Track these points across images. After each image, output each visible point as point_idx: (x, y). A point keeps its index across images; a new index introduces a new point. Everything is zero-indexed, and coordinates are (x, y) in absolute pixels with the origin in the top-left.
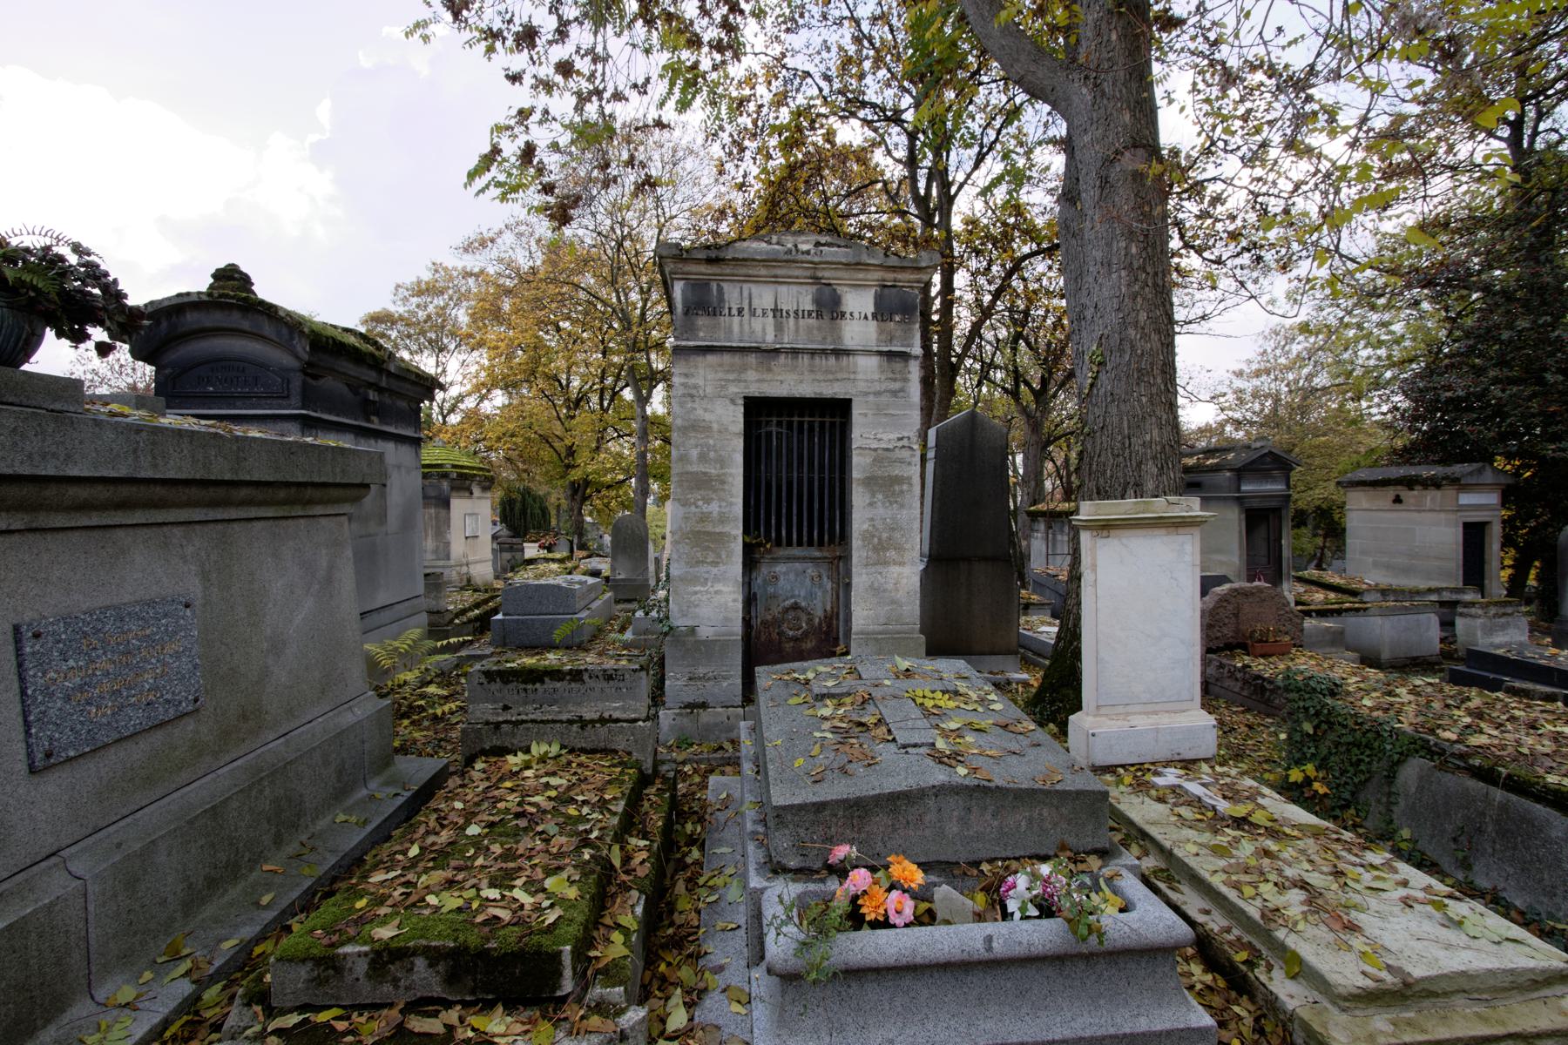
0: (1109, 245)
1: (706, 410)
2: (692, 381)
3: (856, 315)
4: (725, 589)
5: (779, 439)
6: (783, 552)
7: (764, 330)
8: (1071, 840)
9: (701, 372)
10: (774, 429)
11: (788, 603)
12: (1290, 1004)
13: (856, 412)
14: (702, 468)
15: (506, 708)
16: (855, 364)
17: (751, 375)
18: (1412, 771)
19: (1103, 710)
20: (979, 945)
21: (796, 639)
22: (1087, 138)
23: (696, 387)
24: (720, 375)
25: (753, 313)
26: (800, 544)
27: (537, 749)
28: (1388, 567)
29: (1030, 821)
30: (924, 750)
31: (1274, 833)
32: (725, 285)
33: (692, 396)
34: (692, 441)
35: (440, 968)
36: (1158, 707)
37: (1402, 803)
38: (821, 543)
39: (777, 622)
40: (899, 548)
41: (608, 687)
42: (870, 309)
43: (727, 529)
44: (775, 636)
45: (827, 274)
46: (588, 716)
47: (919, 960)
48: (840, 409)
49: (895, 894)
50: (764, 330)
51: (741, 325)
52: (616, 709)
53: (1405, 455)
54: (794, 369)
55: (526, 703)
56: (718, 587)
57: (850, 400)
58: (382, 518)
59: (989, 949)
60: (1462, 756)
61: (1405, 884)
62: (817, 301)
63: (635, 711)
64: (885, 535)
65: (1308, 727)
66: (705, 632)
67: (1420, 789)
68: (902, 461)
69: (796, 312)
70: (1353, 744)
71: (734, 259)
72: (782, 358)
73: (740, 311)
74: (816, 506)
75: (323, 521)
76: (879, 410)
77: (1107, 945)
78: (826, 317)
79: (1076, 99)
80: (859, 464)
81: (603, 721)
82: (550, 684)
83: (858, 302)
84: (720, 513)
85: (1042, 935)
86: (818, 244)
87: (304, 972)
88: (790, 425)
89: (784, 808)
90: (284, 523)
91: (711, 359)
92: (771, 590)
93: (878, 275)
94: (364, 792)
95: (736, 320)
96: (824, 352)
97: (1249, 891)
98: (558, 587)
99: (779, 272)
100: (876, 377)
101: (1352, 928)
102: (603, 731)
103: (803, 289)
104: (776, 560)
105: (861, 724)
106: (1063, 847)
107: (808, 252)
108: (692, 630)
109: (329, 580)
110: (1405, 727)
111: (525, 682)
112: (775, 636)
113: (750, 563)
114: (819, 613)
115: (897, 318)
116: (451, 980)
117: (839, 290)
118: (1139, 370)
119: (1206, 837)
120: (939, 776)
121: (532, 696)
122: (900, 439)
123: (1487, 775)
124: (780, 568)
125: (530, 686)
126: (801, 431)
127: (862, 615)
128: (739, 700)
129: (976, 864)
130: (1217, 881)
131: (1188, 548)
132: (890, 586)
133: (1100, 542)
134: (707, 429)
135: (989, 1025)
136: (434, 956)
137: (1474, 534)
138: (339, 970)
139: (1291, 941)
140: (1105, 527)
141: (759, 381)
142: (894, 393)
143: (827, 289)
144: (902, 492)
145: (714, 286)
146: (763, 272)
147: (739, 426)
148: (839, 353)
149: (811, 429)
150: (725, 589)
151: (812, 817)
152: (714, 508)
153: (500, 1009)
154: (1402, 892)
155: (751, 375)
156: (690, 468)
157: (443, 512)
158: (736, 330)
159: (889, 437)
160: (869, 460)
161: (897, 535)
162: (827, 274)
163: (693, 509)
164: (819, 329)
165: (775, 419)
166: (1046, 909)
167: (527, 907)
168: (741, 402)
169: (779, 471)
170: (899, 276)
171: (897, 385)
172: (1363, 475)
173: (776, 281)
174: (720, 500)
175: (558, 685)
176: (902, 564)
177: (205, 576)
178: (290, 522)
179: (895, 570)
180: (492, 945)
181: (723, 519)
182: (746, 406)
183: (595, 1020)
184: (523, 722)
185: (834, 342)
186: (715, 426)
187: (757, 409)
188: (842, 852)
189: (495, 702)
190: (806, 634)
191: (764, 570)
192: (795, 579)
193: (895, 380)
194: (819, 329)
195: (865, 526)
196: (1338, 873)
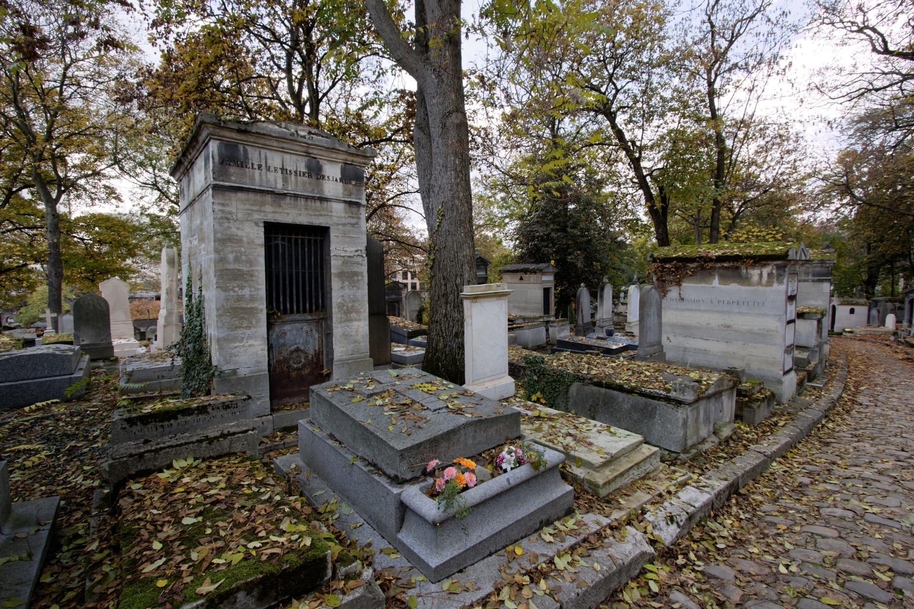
0: (446, 157)
1: (238, 229)
2: (227, 209)
3: (331, 178)
5: (284, 249)
6: (288, 317)
8: (510, 436)
9: (234, 203)
10: (280, 242)
11: (293, 348)
12: (582, 476)
13: (333, 234)
14: (237, 266)
15: (146, 442)
16: (331, 207)
18: (574, 388)
20: (506, 483)
21: (298, 369)
22: (434, 101)
23: (230, 213)
25: (268, 169)
26: (298, 312)
27: (179, 464)
28: (518, 308)
30: (444, 410)
31: (551, 419)
32: (249, 149)
33: (228, 219)
34: (229, 249)
35: (255, 593)
37: (571, 400)
39: (286, 360)
40: (358, 312)
41: (227, 413)
43: (255, 305)
44: (285, 369)
45: (315, 152)
46: (212, 435)
47: (488, 497)
48: (323, 232)
49: (467, 474)
50: (276, 181)
52: (233, 426)
53: (521, 259)
54: (295, 207)
56: (251, 342)
57: (329, 228)
59: (509, 483)
60: (590, 379)
61: (595, 426)
62: (308, 167)
63: (246, 425)
64: (350, 305)
65: (535, 378)
66: (243, 372)
67: (577, 394)
69: (296, 172)
70: (555, 381)
71: (257, 133)
72: (288, 200)
73: (260, 167)
74: (307, 289)
77: (548, 466)
78: (314, 177)
79: (429, 80)
80: (335, 265)
81: (223, 436)
82: (181, 419)
83: (332, 171)
85: (524, 472)
86: (310, 133)
88: (290, 240)
89: (404, 450)
91: (240, 195)
92: (282, 341)
93: (344, 157)
95: (257, 172)
96: (313, 198)
97: (556, 441)
99: (285, 146)
100: (343, 215)
101: (591, 444)
102: (225, 443)
103: (300, 158)
104: (284, 323)
105: (404, 405)
106: (507, 439)
107: (304, 137)
108: (234, 372)
110: (570, 371)
112: (285, 369)
113: (270, 326)
114: (311, 352)
117: (321, 162)
119: (530, 426)
120: (461, 420)
121: (168, 430)
123: (599, 384)
124: (287, 327)
125: (166, 423)
127: (340, 350)
128: (268, 411)
129: (480, 455)
130: (543, 441)
132: (354, 333)
133: (474, 305)
134: (240, 241)
135: (510, 516)
136: (248, 588)
137: (546, 291)
139: (576, 454)
140: (475, 298)
141: (273, 212)
142: (353, 225)
143: (314, 161)
145: (241, 148)
146: (275, 144)
147: (261, 239)
148: (322, 199)
149: (303, 243)
152: (246, 292)
153: (295, 601)
154: (595, 429)
155: (268, 208)
156: (228, 266)
158: (258, 179)
159: (350, 250)
160: (340, 262)
161: (356, 304)
162: (315, 152)
163: (232, 293)
164: (310, 184)
165: (280, 236)
166: (519, 462)
167: (286, 543)
168: (262, 225)
169: (284, 268)
170: (355, 159)
171: (354, 221)
172: (508, 267)
173: (283, 151)
174: (250, 287)
175: (189, 418)
176: (359, 320)
179: (356, 324)
180: (285, 566)
182: (265, 227)
183: (351, 583)
184: (161, 449)
186: (245, 239)
187: (272, 229)
188: (434, 463)
190: (304, 366)
191: (277, 329)
192: (298, 334)
193: (353, 218)
196: (576, 428)
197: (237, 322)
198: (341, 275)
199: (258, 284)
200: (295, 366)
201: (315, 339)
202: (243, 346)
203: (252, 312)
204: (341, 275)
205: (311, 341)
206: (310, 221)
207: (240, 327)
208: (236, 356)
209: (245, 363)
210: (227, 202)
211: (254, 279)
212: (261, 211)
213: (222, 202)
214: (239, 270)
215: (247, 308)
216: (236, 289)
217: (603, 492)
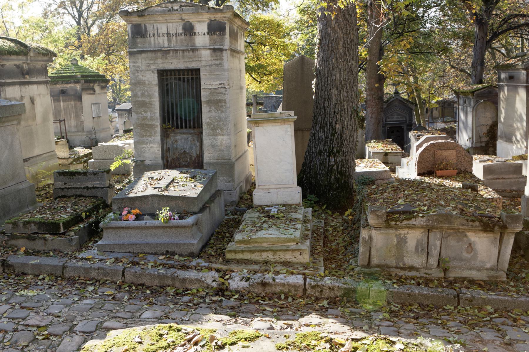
1: (143, 76)
2: (137, 65)
3: (200, 33)
4: (155, 146)
7: (163, 42)
9: (140, 60)
10: (173, 81)
15: (65, 184)
16: (201, 54)
17: (160, 61)
19: (260, 187)
23: (138, 67)
24: (148, 62)
26: (186, 127)
29: (176, 204)
33: (137, 71)
34: (138, 89)
36: (281, 186)
38: (194, 128)
42: (206, 30)
43: (154, 123)
46: (89, 186)
50: (163, 42)
51: (154, 40)
55: (70, 182)
56: (152, 145)
58: (34, 118)
64: (216, 124)
68: (221, 93)
73: (154, 35)
76: (211, 73)
80: (204, 95)
81: (94, 188)
84: (151, 116)
87: (11, 225)
92: (175, 146)
94: (28, 209)
95: (152, 38)
96: (187, 50)
98: (118, 146)
100: (210, 59)
102: (94, 190)
103: (178, 24)
113: (165, 134)
114: (195, 155)
115: (217, 34)
116: (39, 228)
117: (193, 23)
118: (332, 47)
122: (221, 84)
124: (178, 137)
131: (289, 130)
132: (219, 144)
134: (144, 83)
138: (17, 226)
142: (217, 65)
152: (148, 114)
155: (160, 61)
157: (78, 104)
158: (153, 42)
160: (208, 93)
161: (221, 123)
163: (140, 115)
164: (185, 40)
168: (156, 72)
171: (217, 62)
175: (80, 177)
176: (223, 135)
179: (220, 138)
182: (158, 73)
184: (70, 188)
185: (192, 46)
186: (147, 82)
187: (163, 74)
189: (61, 182)
193: (217, 60)
194: (185, 40)
195: (208, 120)
200: (183, 163)
202: (148, 147)
204: (209, 102)
205: (194, 147)
206: (186, 66)
207: (145, 136)
208: (144, 153)
209: (149, 158)
211: (153, 106)
214: (144, 101)
216: (143, 113)
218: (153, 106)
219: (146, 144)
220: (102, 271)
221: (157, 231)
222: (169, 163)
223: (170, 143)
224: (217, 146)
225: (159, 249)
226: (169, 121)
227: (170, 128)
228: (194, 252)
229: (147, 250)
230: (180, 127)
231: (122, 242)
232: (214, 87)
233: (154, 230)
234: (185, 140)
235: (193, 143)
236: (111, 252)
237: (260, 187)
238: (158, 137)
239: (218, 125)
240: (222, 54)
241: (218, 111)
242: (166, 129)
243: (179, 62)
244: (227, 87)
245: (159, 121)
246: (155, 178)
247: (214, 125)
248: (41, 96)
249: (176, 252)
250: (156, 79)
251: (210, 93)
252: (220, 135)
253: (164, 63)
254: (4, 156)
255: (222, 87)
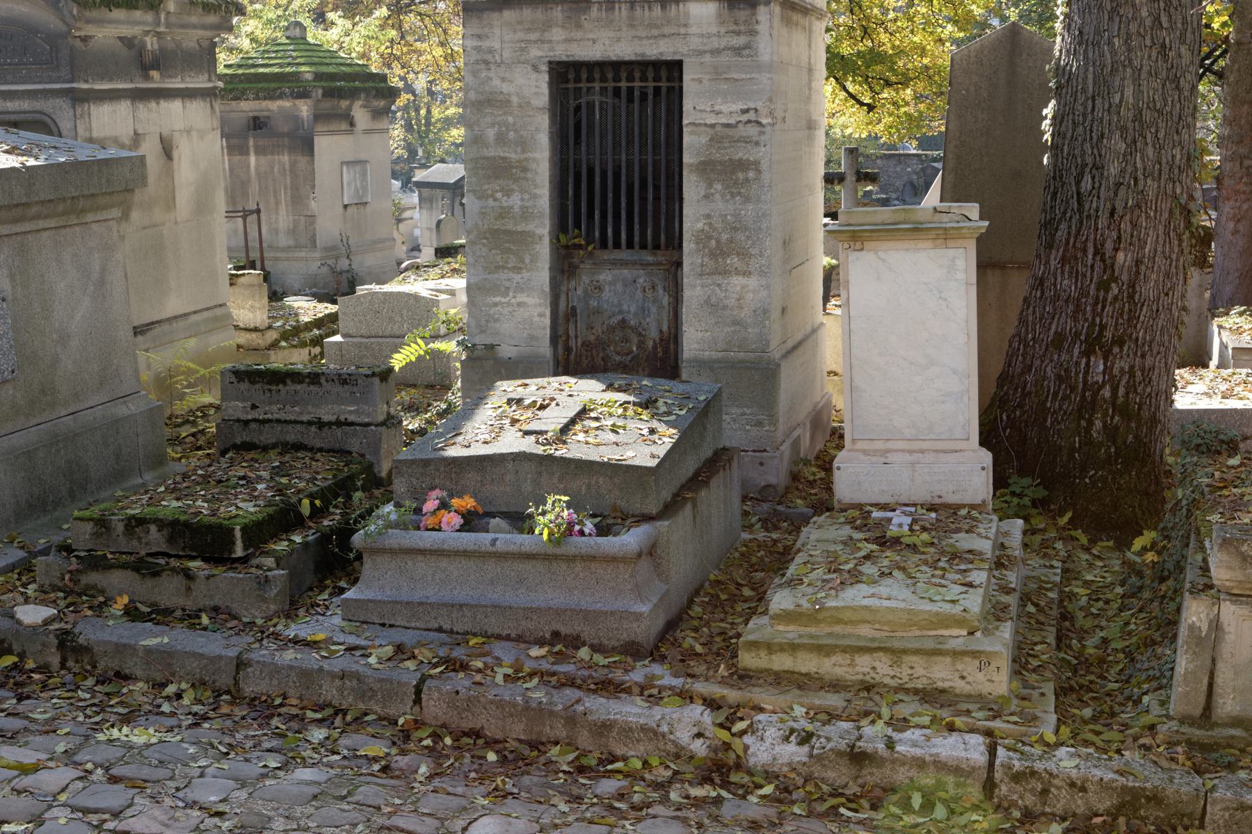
1: (503, 80)
2: (486, 44)
4: (530, 301)
6: (606, 255)
9: (497, 31)
10: (597, 99)
11: (615, 320)
15: (254, 407)
16: (687, 14)
17: (557, 34)
19: (859, 445)
23: (491, 51)
24: (520, 35)
26: (630, 245)
29: (589, 486)
33: (487, 63)
34: (488, 120)
36: (925, 445)
38: (657, 247)
41: (344, 391)
43: (530, 227)
46: (326, 418)
48: (668, 73)
52: (351, 412)
56: (522, 298)
58: (170, 202)
63: (368, 415)
64: (725, 237)
68: (747, 141)
75: (95, 227)
76: (717, 74)
80: (693, 144)
81: (339, 423)
82: (292, 387)
84: (522, 207)
90: (63, 231)
94: (140, 481)
98: (416, 297)
100: (714, 30)
109: (102, 282)
111: (269, 383)
114: (654, 334)
116: (171, 540)
124: (605, 276)
126: (630, 100)
131: (961, 263)
132: (732, 302)
142: (738, 51)
144: (747, 180)
149: (644, 97)
150: (530, 301)
151: (420, 470)
152: (515, 201)
155: (557, 34)
157: (302, 161)
160: (704, 140)
161: (741, 236)
163: (491, 202)
168: (545, 68)
171: (740, 41)
174: (523, 191)
175: (299, 387)
176: (747, 274)
177: (12, 277)
178: (68, 230)
179: (737, 281)
181: (526, 215)
184: (269, 421)
186: (515, 100)
187: (565, 75)
189: (244, 401)
192: (617, 285)
193: (738, 33)
195: (700, 225)
197: (498, 258)
198: (706, 168)
199: (536, 186)
200: (618, 358)
201: (661, 307)
202: (508, 304)
203: (525, 239)
204: (706, 168)
205: (654, 310)
206: (639, 50)
207: (503, 267)
208: (497, 320)
210: (486, 30)
211: (529, 175)
212: (543, 42)
213: (478, 31)
214: (504, 159)
215: (517, 232)
216: (499, 195)
217: (747, 659)
218: (529, 175)
219: (506, 294)
220: (355, 682)
221: (528, 566)
222: (572, 357)
223: (579, 292)
224: (725, 307)
225: (531, 625)
226: (577, 225)
227: (579, 247)
228: (639, 639)
229: (493, 625)
230: (610, 243)
231: (417, 596)
232: (724, 121)
233: (519, 566)
234: (625, 285)
235: (649, 294)
236: (383, 625)
237: (859, 445)
238: (542, 275)
239: (731, 241)
240: (754, 14)
241: (733, 196)
242: (566, 247)
243: (619, 40)
244: (764, 121)
245: (547, 222)
246: (527, 402)
247: (718, 242)
248: (194, 134)
249: (585, 636)
250: (545, 89)
251: (711, 140)
252: (738, 272)
253: (569, 41)
254: (78, 317)
255: (749, 122)
